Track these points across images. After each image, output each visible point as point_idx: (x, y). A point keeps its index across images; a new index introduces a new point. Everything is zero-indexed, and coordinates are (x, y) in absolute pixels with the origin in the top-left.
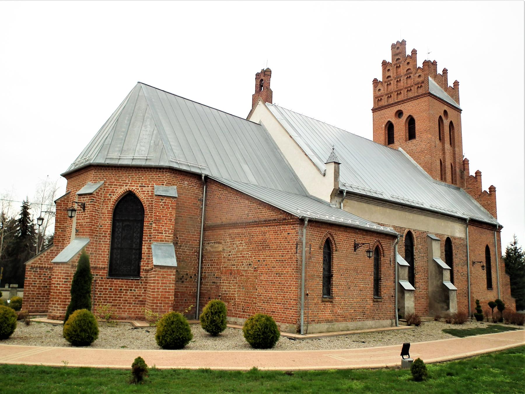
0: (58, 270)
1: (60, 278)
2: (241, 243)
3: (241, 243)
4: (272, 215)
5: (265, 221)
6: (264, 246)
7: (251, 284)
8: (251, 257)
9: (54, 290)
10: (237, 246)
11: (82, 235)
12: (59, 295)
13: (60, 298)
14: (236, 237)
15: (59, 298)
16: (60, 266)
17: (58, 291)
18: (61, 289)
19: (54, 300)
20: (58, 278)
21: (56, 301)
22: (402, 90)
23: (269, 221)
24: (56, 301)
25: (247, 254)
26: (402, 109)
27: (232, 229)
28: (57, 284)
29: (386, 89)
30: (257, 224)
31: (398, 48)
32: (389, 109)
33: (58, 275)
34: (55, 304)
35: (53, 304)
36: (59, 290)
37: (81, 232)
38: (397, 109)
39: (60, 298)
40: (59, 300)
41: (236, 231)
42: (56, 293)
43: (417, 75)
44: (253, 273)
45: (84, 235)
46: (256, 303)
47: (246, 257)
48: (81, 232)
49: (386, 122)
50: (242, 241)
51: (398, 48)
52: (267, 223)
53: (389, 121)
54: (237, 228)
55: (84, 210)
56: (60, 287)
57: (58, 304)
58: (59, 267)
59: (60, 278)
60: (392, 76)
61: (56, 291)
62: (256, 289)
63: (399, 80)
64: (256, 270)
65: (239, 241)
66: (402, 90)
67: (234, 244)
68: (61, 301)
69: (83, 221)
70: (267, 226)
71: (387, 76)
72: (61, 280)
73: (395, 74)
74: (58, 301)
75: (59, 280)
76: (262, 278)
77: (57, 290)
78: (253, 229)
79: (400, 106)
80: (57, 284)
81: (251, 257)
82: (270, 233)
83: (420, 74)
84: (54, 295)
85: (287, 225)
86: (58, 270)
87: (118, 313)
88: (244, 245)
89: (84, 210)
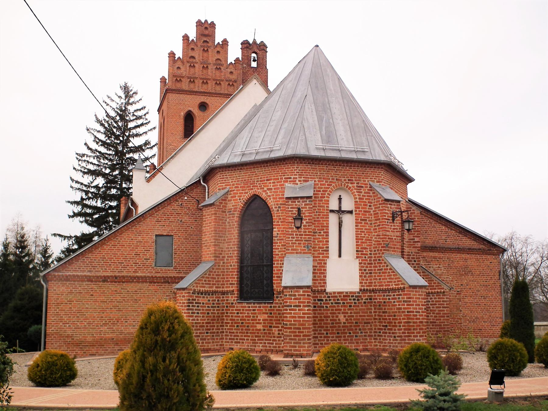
0: (415, 295)
1: (419, 305)
2: (439, 267)
3: (439, 267)
4: (475, 245)
5: (469, 249)
6: (466, 271)
7: (454, 306)
8: (452, 281)
9: (413, 319)
10: (434, 270)
11: (393, 251)
12: (420, 326)
13: (422, 329)
14: (432, 260)
15: (420, 329)
16: (418, 290)
17: (418, 321)
18: (421, 317)
19: (415, 331)
20: (416, 305)
21: (417, 333)
22: (209, 79)
23: (474, 249)
24: (417, 333)
25: (447, 278)
26: (208, 102)
27: (426, 252)
28: (416, 312)
29: (188, 71)
30: (459, 250)
31: (206, 29)
32: (191, 96)
33: (416, 302)
34: (417, 336)
35: (414, 336)
36: (419, 319)
37: (391, 248)
38: (202, 100)
39: (422, 329)
40: (421, 331)
41: (431, 254)
42: (417, 322)
43: (229, 70)
44: (456, 296)
45: (395, 251)
46: (461, 323)
47: (446, 281)
48: (391, 248)
49: (186, 110)
50: (440, 265)
51: (206, 28)
52: (470, 251)
53: (190, 111)
54: (434, 252)
55: (393, 220)
56: (419, 315)
57: (420, 336)
58: (416, 292)
59: (419, 305)
60: (197, 57)
61: (415, 321)
62: (461, 311)
63: (205, 66)
64: (459, 293)
65: (436, 265)
66: (209, 79)
67: (430, 267)
68: (423, 333)
69: (392, 234)
70: (468, 254)
71: (190, 55)
72: (421, 307)
73: (201, 58)
74: (419, 333)
75: (418, 307)
76: (466, 300)
77: (417, 319)
78: (453, 255)
79: (206, 98)
80: (416, 312)
81: (452, 281)
82: (472, 260)
83: (232, 70)
84: (414, 326)
85: (489, 255)
86: (415, 295)
87: (201, 346)
88: (443, 269)
89: (393, 220)
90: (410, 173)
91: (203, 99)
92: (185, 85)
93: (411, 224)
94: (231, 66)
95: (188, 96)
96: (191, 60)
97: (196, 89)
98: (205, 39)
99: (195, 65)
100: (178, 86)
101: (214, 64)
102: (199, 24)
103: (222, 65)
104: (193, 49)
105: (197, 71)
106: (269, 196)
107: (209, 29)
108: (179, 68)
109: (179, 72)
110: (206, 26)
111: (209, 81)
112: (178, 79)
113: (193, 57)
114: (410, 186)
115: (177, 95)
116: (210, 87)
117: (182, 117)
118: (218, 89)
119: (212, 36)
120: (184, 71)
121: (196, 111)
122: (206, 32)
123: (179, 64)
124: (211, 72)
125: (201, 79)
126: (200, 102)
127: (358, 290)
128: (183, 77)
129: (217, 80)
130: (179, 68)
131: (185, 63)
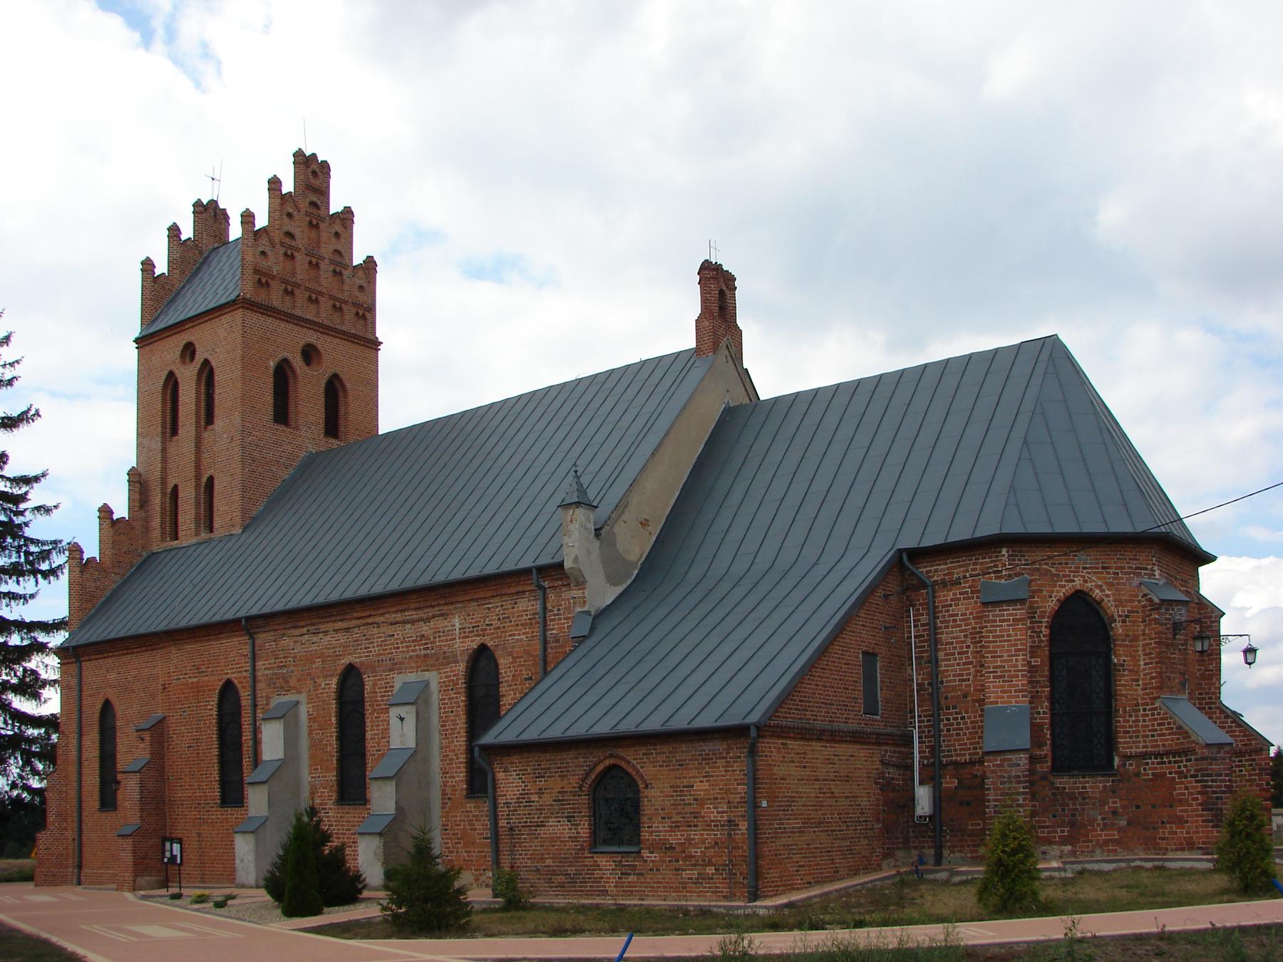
26: (319, 346)
43: (358, 282)
49: (280, 357)
51: (314, 173)
71: (285, 229)
90: (1205, 545)
91: (311, 337)
92: (275, 298)
93: (1206, 643)
94: (361, 273)
95: (283, 325)
96: (288, 241)
97: (298, 312)
98: (314, 199)
99: (296, 254)
100: (262, 297)
101: (332, 262)
102: (299, 155)
103: (346, 266)
104: (290, 215)
105: (297, 270)
106: (1108, 596)
107: (321, 177)
108: (263, 253)
109: (264, 264)
110: (314, 167)
111: (297, 292)
112: (264, 281)
113: (290, 235)
114: (1203, 571)
115: (262, 318)
116: (324, 313)
117: (271, 371)
118: (334, 321)
119: (324, 192)
120: (275, 263)
121: (297, 362)
122: (316, 183)
123: (264, 244)
124: (326, 279)
125: (307, 289)
126: (302, 343)
127: (957, 748)
128: (273, 278)
129: (336, 299)
130: (263, 253)
131: (278, 246)
